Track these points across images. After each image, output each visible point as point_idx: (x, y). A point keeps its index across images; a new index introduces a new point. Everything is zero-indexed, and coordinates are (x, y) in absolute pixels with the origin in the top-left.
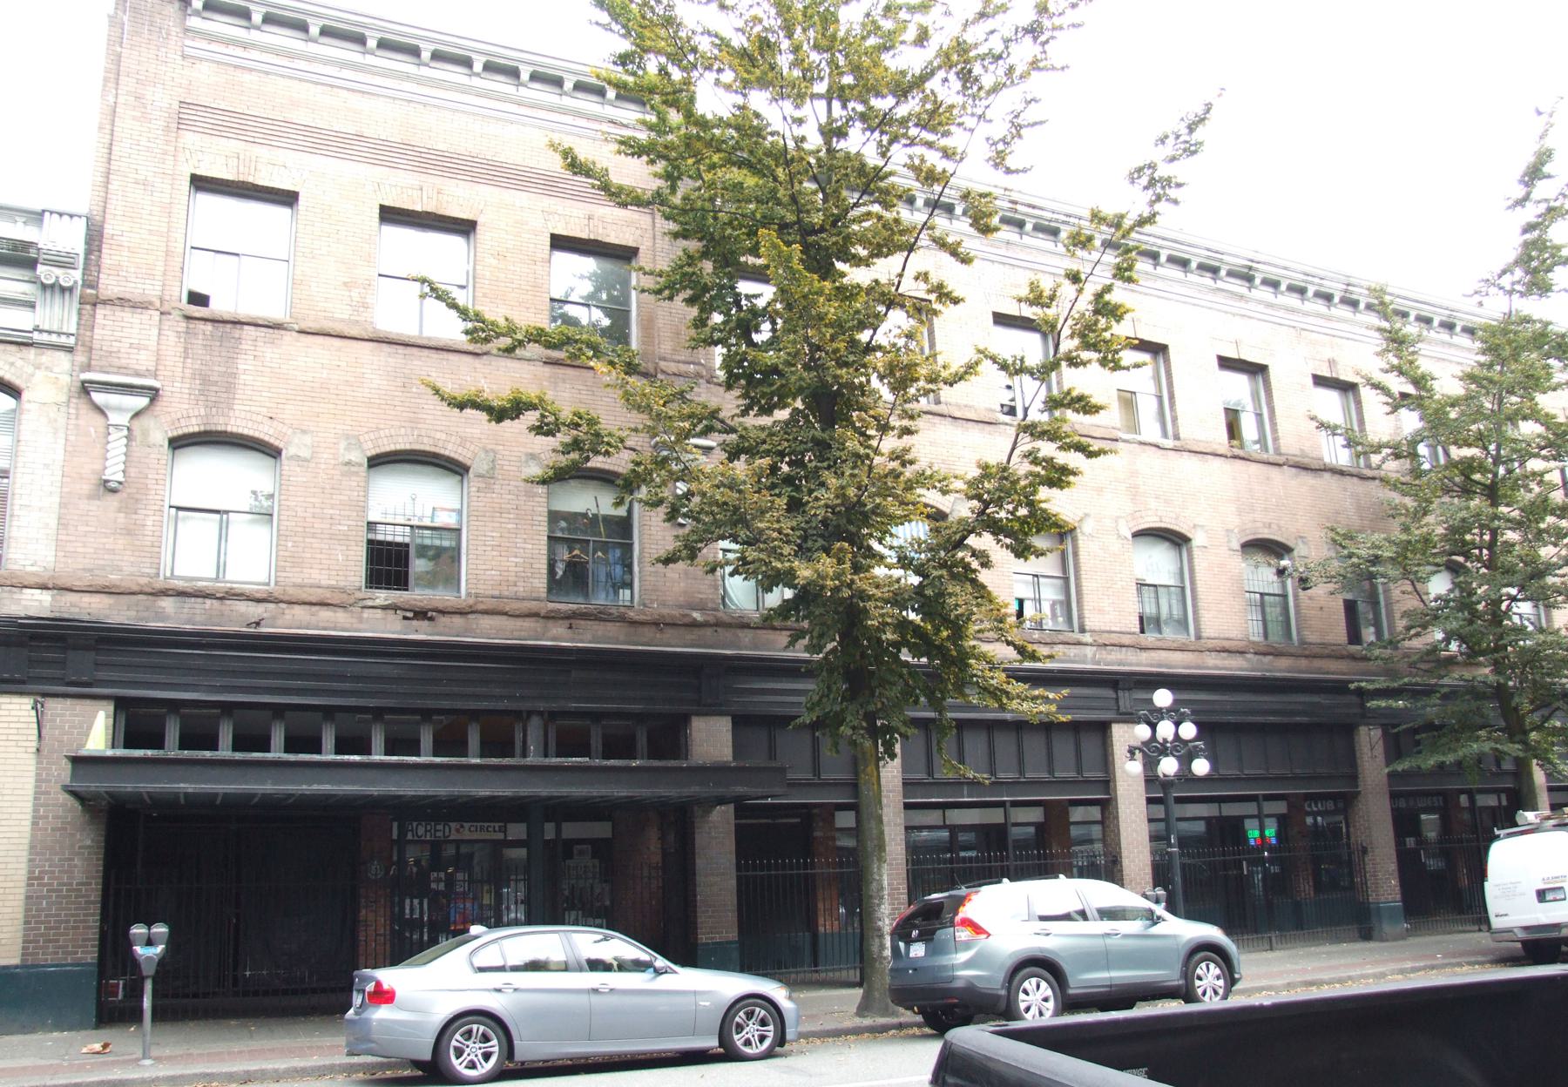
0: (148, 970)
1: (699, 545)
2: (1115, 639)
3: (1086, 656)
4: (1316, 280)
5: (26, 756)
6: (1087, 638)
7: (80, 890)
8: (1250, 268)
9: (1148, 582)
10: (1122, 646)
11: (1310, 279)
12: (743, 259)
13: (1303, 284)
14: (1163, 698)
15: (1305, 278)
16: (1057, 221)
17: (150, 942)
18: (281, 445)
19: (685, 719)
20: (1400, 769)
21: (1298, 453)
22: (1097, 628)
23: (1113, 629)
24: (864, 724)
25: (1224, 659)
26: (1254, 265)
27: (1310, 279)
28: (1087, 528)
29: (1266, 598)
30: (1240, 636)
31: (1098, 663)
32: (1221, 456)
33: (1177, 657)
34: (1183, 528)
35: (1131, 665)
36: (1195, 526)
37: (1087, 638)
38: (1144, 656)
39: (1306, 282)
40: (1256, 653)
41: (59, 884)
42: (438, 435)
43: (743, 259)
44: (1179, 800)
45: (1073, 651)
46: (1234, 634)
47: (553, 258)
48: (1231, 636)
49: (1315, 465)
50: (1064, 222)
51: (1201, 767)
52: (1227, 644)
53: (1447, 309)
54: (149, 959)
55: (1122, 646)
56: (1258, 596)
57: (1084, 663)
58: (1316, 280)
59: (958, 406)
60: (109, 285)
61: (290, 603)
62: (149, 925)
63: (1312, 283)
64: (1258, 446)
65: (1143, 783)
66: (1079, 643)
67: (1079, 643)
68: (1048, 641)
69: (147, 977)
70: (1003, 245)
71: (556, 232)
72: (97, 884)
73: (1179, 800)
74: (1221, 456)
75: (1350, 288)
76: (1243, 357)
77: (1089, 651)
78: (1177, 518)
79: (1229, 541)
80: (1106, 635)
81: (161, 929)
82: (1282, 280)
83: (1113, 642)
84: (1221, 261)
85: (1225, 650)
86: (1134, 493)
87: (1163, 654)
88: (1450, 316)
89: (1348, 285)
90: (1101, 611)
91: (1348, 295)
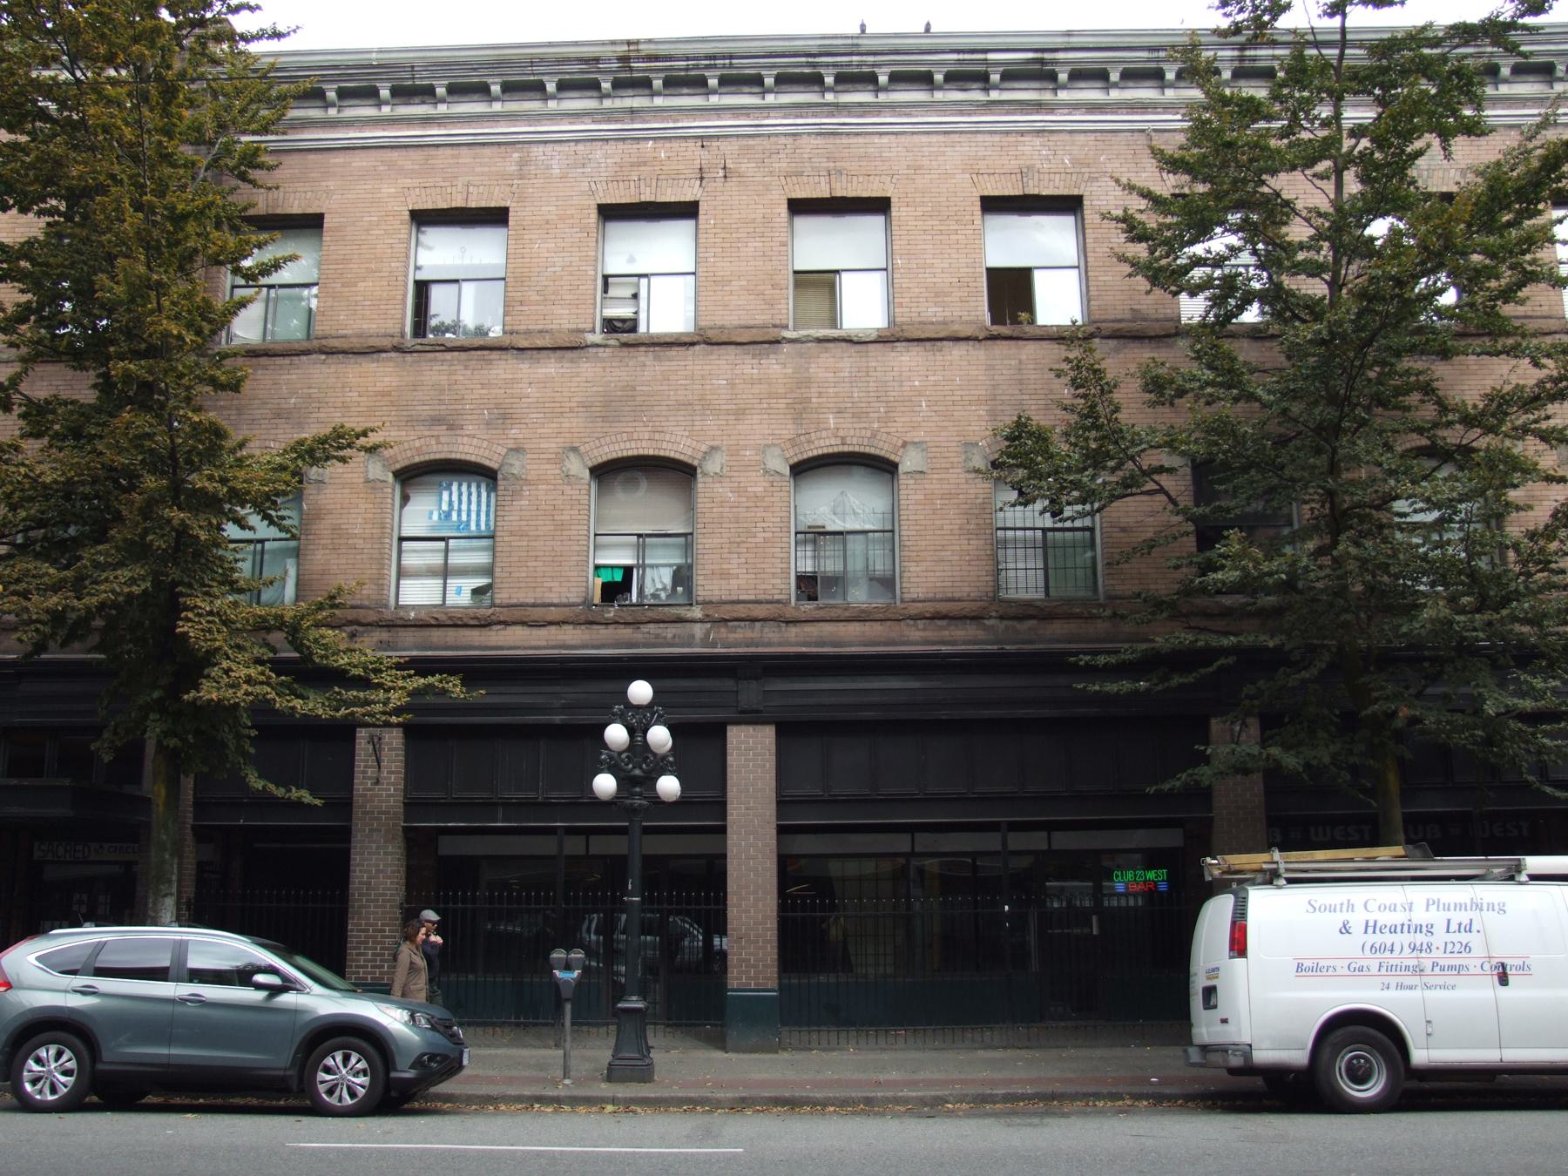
0: (566, 993)
1: (86, 542)
2: (741, 611)
3: (693, 636)
6: (697, 613)
8: (1042, 61)
9: (830, 528)
10: (754, 620)
13: (1153, 65)
14: (640, 691)
15: (1039, 55)
16: (697, 67)
17: (568, 967)
18: (897, 459)
21: (1128, 316)
22: (714, 599)
23: (742, 598)
25: (942, 628)
26: (1047, 56)
28: (713, 466)
29: (1050, 534)
30: (579, 600)
31: (714, 645)
32: (967, 339)
33: (854, 630)
34: (882, 449)
35: (770, 644)
36: (905, 444)
37: (697, 613)
38: (793, 632)
40: (1002, 618)
42: (417, 444)
44: (647, 831)
45: (670, 631)
46: (963, 591)
47: (986, 224)
48: (957, 595)
49: (1157, 329)
50: (707, 67)
52: (944, 607)
54: (567, 982)
55: (754, 620)
56: (1039, 534)
57: (690, 645)
59: (528, 332)
61: (787, 622)
62: (568, 950)
65: (774, 805)
66: (680, 620)
67: (680, 620)
68: (630, 619)
69: (567, 1000)
70: (628, 116)
71: (986, 194)
72: (353, 907)
73: (647, 831)
74: (967, 339)
76: (839, 194)
77: (698, 630)
78: (874, 436)
79: (967, 460)
80: (728, 607)
81: (578, 955)
82: (1165, 66)
83: (735, 615)
84: (1055, 62)
85: (936, 616)
86: (800, 410)
87: (827, 628)
90: (725, 575)
91: (1247, 64)
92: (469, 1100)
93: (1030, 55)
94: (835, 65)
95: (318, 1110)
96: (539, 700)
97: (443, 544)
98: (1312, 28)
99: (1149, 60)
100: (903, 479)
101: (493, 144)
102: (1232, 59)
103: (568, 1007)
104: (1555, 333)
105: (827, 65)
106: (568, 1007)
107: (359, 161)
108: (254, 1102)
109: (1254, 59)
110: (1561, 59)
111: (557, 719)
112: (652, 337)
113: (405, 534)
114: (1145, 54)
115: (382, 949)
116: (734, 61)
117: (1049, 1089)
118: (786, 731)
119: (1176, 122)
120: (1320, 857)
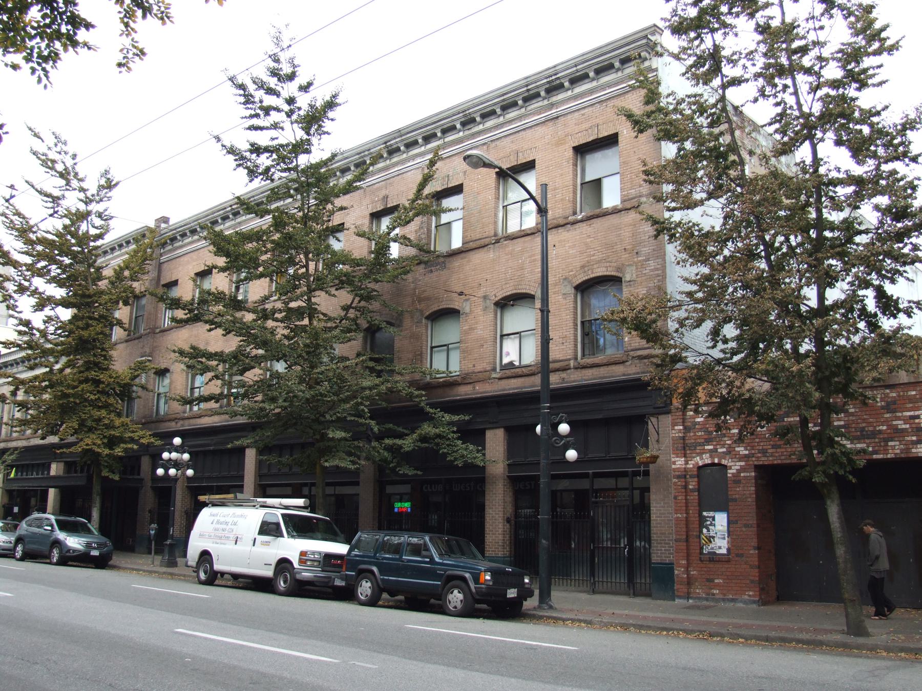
4: (367, 153)
5: (751, 533)
7: (669, 547)
11: (362, 154)
12: (355, 185)
13: (362, 160)
19: (9, 501)
20: (110, 477)
24: (723, 417)
27: (362, 154)
39: (362, 157)
41: (657, 547)
43: (355, 185)
51: (190, 472)
53: (459, 113)
58: (367, 153)
60: (552, 237)
63: (365, 156)
64: (396, 315)
75: (388, 144)
88: (465, 116)
89: (385, 143)
91: (390, 148)
92: (556, 619)
93: (357, 156)
94: (403, 140)
95: (441, 610)
96: (206, 442)
97: (446, 347)
98: (238, 198)
99: (360, 158)
100: (624, 284)
101: (521, 130)
102: (384, 148)
103: (153, 542)
104: (582, 221)
105: (476, 112)
106: (153, 542)
107: (185, 258)
108: (75, 564)
109: (391, 145)
110: (497, 106)
111: (212, 448)
112: (454, 250)
113: (505, 332)
114: (357, 156)
115: (657, 547)
116: (578, 67)
117: (640, 623)
118: (509, 430)
119: (271, 220)
120: (172, 494)
